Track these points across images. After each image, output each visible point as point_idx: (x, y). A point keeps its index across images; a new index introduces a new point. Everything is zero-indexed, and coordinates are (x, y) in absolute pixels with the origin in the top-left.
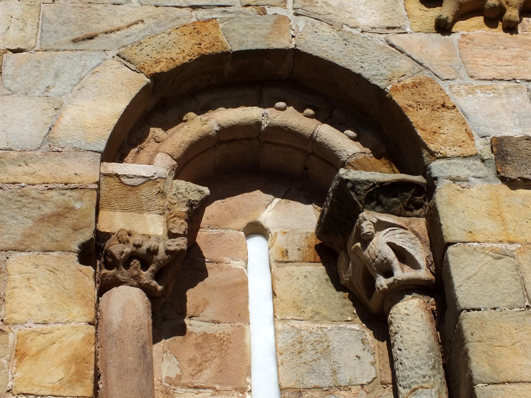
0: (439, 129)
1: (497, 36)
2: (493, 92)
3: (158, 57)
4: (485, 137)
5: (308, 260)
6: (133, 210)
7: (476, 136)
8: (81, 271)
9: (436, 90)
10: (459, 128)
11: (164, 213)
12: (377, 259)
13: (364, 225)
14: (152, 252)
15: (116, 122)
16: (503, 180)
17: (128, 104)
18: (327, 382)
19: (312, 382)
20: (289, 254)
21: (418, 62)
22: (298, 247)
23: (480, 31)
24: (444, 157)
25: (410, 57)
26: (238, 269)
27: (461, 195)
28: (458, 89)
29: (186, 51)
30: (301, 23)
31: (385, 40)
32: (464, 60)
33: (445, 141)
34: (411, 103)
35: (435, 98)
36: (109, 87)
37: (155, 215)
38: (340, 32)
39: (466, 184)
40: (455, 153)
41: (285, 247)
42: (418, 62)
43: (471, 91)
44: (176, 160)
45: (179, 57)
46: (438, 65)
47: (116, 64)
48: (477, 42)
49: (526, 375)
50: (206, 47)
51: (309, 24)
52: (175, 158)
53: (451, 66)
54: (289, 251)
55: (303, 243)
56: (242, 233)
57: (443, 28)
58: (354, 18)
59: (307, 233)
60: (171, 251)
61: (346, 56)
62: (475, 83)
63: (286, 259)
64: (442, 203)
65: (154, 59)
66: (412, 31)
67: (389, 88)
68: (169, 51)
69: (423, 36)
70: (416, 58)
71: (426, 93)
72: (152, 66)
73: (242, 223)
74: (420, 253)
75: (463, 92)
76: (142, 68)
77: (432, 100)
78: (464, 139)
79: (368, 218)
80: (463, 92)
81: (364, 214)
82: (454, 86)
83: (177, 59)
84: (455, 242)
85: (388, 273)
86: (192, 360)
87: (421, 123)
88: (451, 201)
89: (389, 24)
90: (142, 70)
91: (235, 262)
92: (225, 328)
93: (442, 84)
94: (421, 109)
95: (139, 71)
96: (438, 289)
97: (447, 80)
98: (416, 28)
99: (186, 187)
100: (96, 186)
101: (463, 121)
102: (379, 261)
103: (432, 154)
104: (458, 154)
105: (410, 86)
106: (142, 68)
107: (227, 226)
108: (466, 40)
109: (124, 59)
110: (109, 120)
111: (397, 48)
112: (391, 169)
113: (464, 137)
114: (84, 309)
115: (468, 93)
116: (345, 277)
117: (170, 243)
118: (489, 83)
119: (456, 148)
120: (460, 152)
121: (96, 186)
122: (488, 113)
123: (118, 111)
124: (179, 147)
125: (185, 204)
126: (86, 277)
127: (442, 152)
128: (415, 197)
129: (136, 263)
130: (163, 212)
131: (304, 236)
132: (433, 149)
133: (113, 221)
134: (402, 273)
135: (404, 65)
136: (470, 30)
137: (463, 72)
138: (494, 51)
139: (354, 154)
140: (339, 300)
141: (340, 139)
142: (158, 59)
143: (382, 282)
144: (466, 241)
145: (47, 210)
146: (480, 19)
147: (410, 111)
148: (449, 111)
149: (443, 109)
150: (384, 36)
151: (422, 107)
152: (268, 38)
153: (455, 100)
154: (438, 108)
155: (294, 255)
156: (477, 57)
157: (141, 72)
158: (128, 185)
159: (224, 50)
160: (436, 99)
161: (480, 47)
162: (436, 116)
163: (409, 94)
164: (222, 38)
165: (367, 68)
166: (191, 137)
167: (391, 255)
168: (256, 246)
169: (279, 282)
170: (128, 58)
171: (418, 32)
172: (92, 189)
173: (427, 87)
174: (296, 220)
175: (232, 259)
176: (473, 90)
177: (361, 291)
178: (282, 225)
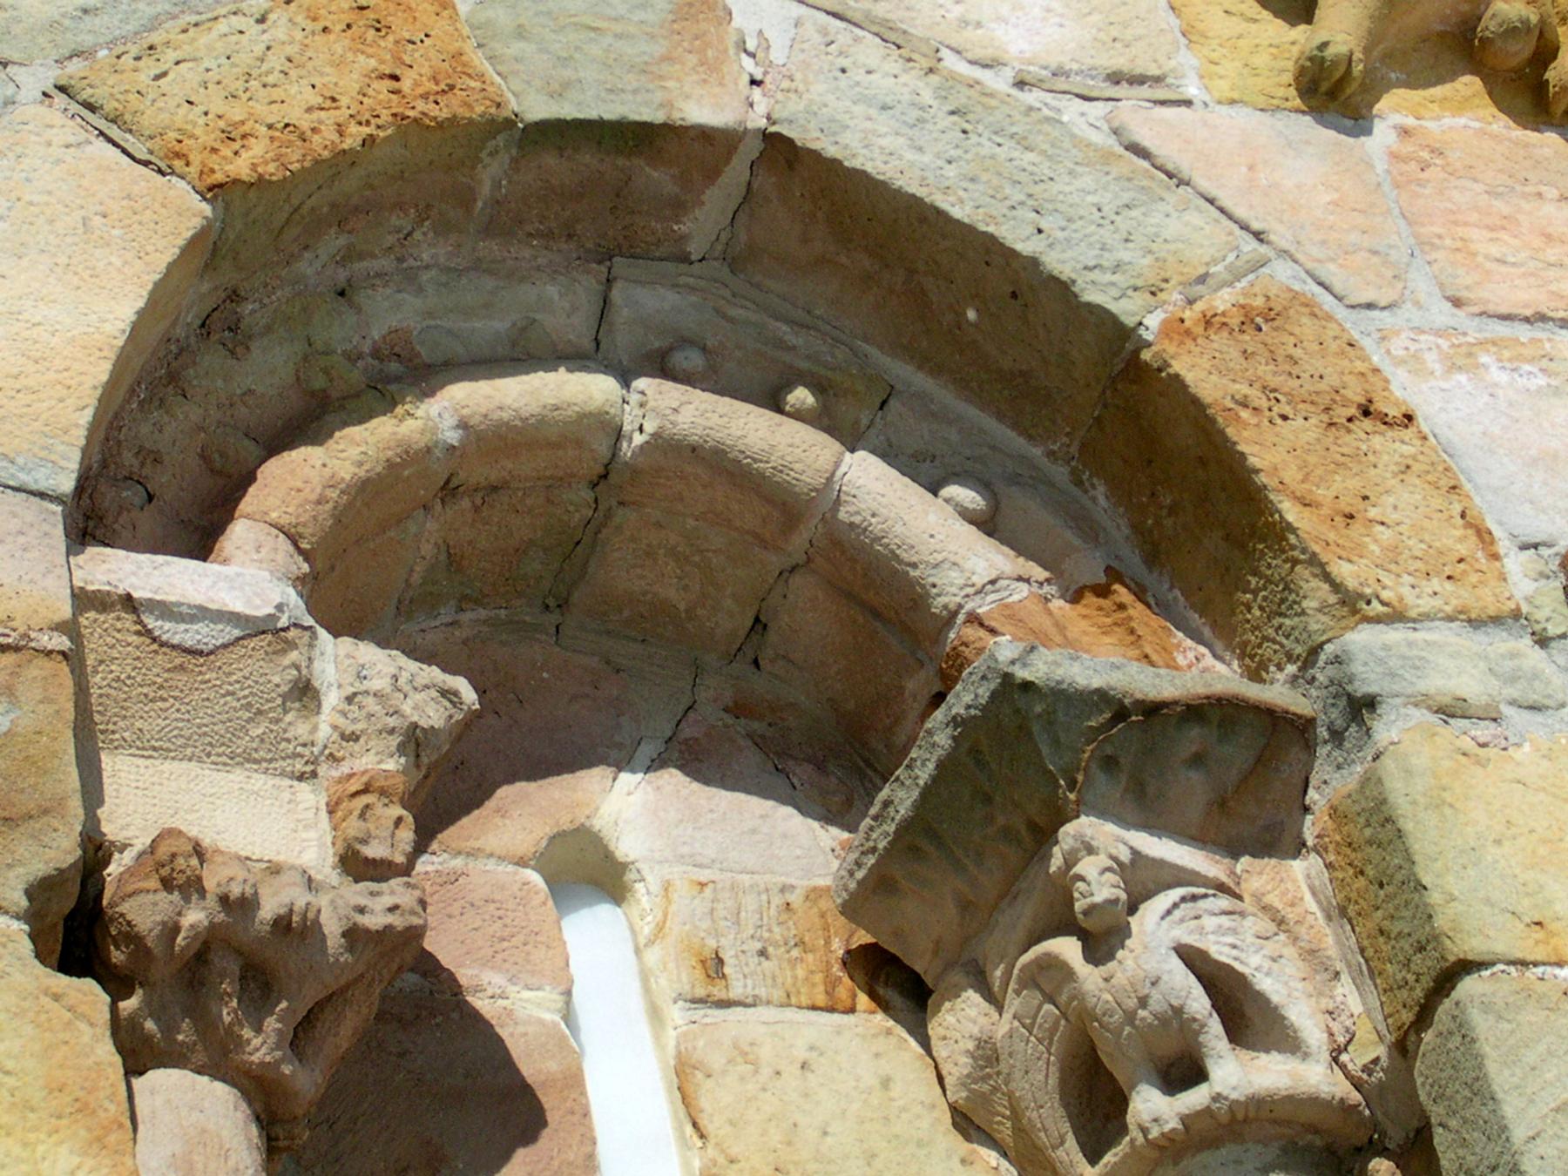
0: (1361, 505)
1: (1526, 145)
2: (1542, 370)
3: (236, 112)
4: (1535, 546)
5: (805, 1001)
6: (189, 751)
7: (1504, 545)
8: (56, 998)
9: (1334, 346)
10: (1437, 502)
11: (314, 774)
12: (1142, 1013)
13: (1088, 867)
15: (105, 378)
17: (141, 304)
20: (727, 970)
21: (1244, 227)
22: (759, 946)
23: (1463, 121)
24: (1396, 616)
25: (1211, 201)
26: (541, 1022)
27: (1479, 771)
28: (1413, 347)
29: (344, 101)
31: (1105, 127)
32: (1422, 230)
33: (1393, 554)
34: (1242, 389)
35: (1333, 379)
36: (51, 222)
37: (277, 781)
38: (934, 79)
39: (1484, 731)
40: (1437, 602)
41: (712, 943)
42: (1244, 227)
43: (1462, 360)
45: (321, 122)
46: (1324, 242)
47: (60, 124)
48: (1458, 165)
50: (420, 91)
51: (809, 30)
52: (305, 546)
53: (1376, 253)
54: (727, 956)
55: (776, 929)
56: (535, 878)
57: (1332, 94)
58: (979, 25)
59: (783, 889)
60: (367, 931)
61: (972, 180)
62: (1475, 330)
63: (718, 992)
64: (1414, 803)
65: (222, 124)
66: (1207, 98)
67: (1153, 321)
68: (277, 94)
69: (1244, 119)
70: (1240, 212)
71: (1297, 353)
72: (214, 150)
75: (1431, 359)
76: (178, 155)
77: (1323, 386)
78: (1463, 550)
80: (1431, 359)
81: (1084, 826)
82: (1397, 333)
83: (314, 130)
84: (1486, 958)
87: (1291, 475)
88: (1447, 795)
89: (1120, 62)
90: (178, 164)
91: (527, 994)
93: (1354, 324)
94: (1285, 418)
95: (166, 162)
97: (1370, 306)
98: (1223, 88)
99: (393, 670)
100: (62, 642)
102: (1150, 1019)
104: (1448, 609)
105: (1234, 322)
106: (178, 155)
107: (477, 844)
108: (1420, 156)
109: (92, 108)
110: (76, 366)
111: (1159, 162)
112: (1135, 653)
113: (1462, 539)
114: (90, 1162)
115: (1453, 368)
117: (363, 901)
118: (1524, 332)
119: (1435, 584)
120: (1454, 602)
121: (62, 642)
122: (1533, 452)
123: (108, 328)
124: (319, 502)
125: (395, 741)
126: (83, 1026)
127: (1385, 595)
130: (309, 768)
131: (777, 900)
132: (1351, 584)
133: (145, 800)
135: (1193, 236)
136: (1422, 112)
137: (1421, 283)
138: (1526, 206)
139: (993, 582)
141: (932, 518)
142: (235, 125)
143: (1153, 1108)
144: (1530, 958)
147: (1246, 425)
148: (1390, 434)
149: (1367, 424)
150: (1098, 109)
151: (1287, 410)
152: (661, 77)
153: (1403, 389)
154: (1350, 420)
156: (1466, 224)
157: (173, 173)
158: (174, 647)
159: (493, 110)
160: (1337, 383)
161: (1469, 184)
162: (1345, 450)
163: (1234, 353)
164: (476, 62)
165: (1060, 235)
166: (360, 464)
168: (594, 937)
169: (709, 1083)
170: (110, 106)
171: (1232, 102)
172: (49, 653)
173: (1297, 330)
175: (512, 980)
176: (1470, 355)
178: (685, 850)
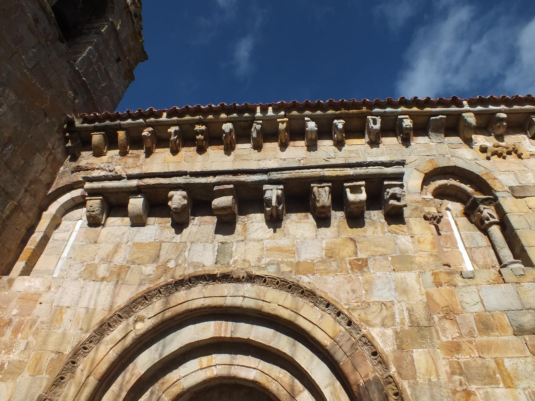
14: (436, 217)
16: (514, 197)
18: (476, 246)
19: (473, 246)
30: (454, 159)
43: (500, 175)
44: (266, 190)
47: (415, 171)
49: (534, 244)
57: (488, 158)
73: (445, 208)
79: (481, 207)
81: (480, 206)
85: (488, 220)
86: (444, 241)
95: (422, 172)
101: (500, 182)
103: (495, 191)
116: (474, 220)
129: (432, 219)
134: (492, 220)
140: (472, 226)
145: (413, 207)
146: (496, 156)
153: (497, 177)
155: (459, 215)
167: (489, 216)
177: (479, 223)
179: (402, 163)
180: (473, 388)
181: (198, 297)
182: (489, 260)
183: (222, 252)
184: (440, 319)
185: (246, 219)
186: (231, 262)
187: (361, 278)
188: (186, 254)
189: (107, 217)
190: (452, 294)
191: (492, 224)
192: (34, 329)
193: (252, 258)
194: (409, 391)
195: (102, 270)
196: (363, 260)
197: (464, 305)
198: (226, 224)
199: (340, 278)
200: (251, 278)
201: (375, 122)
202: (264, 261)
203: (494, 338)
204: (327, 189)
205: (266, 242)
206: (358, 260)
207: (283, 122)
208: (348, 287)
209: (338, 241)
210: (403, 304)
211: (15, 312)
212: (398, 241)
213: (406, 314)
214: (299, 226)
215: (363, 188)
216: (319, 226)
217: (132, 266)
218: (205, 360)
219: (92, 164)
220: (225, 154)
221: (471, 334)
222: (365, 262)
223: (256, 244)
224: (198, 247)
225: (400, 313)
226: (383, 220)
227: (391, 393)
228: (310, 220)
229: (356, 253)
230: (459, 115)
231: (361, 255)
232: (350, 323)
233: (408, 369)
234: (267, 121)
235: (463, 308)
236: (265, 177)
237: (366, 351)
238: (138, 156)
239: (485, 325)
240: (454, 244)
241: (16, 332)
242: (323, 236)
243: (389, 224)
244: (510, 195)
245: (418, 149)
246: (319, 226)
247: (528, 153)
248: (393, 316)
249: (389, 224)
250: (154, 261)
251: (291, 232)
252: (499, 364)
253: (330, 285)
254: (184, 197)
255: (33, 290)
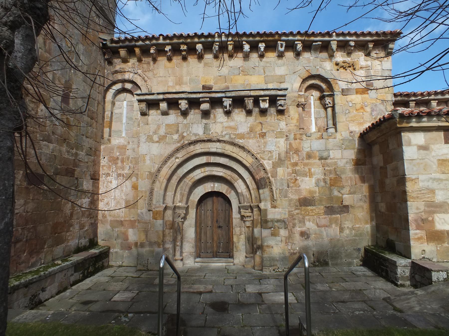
74: (331, 103)
92: (309, 110)
96: (333, 107)
128: (332, 96)
134: (329, 105)
140: (321, 106)
168: (312, 97)
174: (316, 94)
179: (286, 89)
180: (298, 178)
181: (199, 148)
182: (323, 124)
183: (206, 128)
184: (293, 153)
185: (215, 112)
186: (210, 133)
187: (262, 141)
188: (190, 129)
189: (149, 110)
190: (300, 143)
191: (329, 107)
192: (130, 161)
193: (219, 131)
194: (273, 181)
195: (156, 138)
196: (264, 133)
197: (303, 148)
198: (206, 114)
199: (254, 140)
200: (219, 141)
201: (282, 47)
202: (224, 133)
203: (312, 161)
204: (252, 101)
205: (224, 124)
206: (262, 133)
207: (230, 44)
208: (257, 145)
209: (255, 123)
210: (277, 152)
211: (118, 154)
212: (280, 124)
213: (277, 155)
214: (239, 116)
215: (268, 101)
216: (247, 116)
217: (168, 135)
218: (203, 169)
219: (123, 68)
220: (199, 62)
221: (303, 160)
222: (265, 134)
223: (220, 124)
224: (195, 126)
225: (275, 156)
226: (275, 113)
227: (268, 182)
228: (244, 113)
229: (262, 130)
230: (329, 42)
231: (264, 131)
232: (256, 159)
233: (275, 175)
234: (221, 42)
235: (303, 149)
236: (223, 95)
237: (262, 169)
238: (149, 63)
239: (309, 156)
240: (310, 116)
241: (122, 162)
242: (249, 121)
243: (277, 115)
244: (341, 93)
245: (304, 62)
246: (247, 116)
247: (360, 66)
248: (272, 156)
249: (277, 115)
250: (177, 133)
251: (235, 119)
252: (310, 170)
253: (251, 144)
254: (186, 104)
255: (122, 144)
